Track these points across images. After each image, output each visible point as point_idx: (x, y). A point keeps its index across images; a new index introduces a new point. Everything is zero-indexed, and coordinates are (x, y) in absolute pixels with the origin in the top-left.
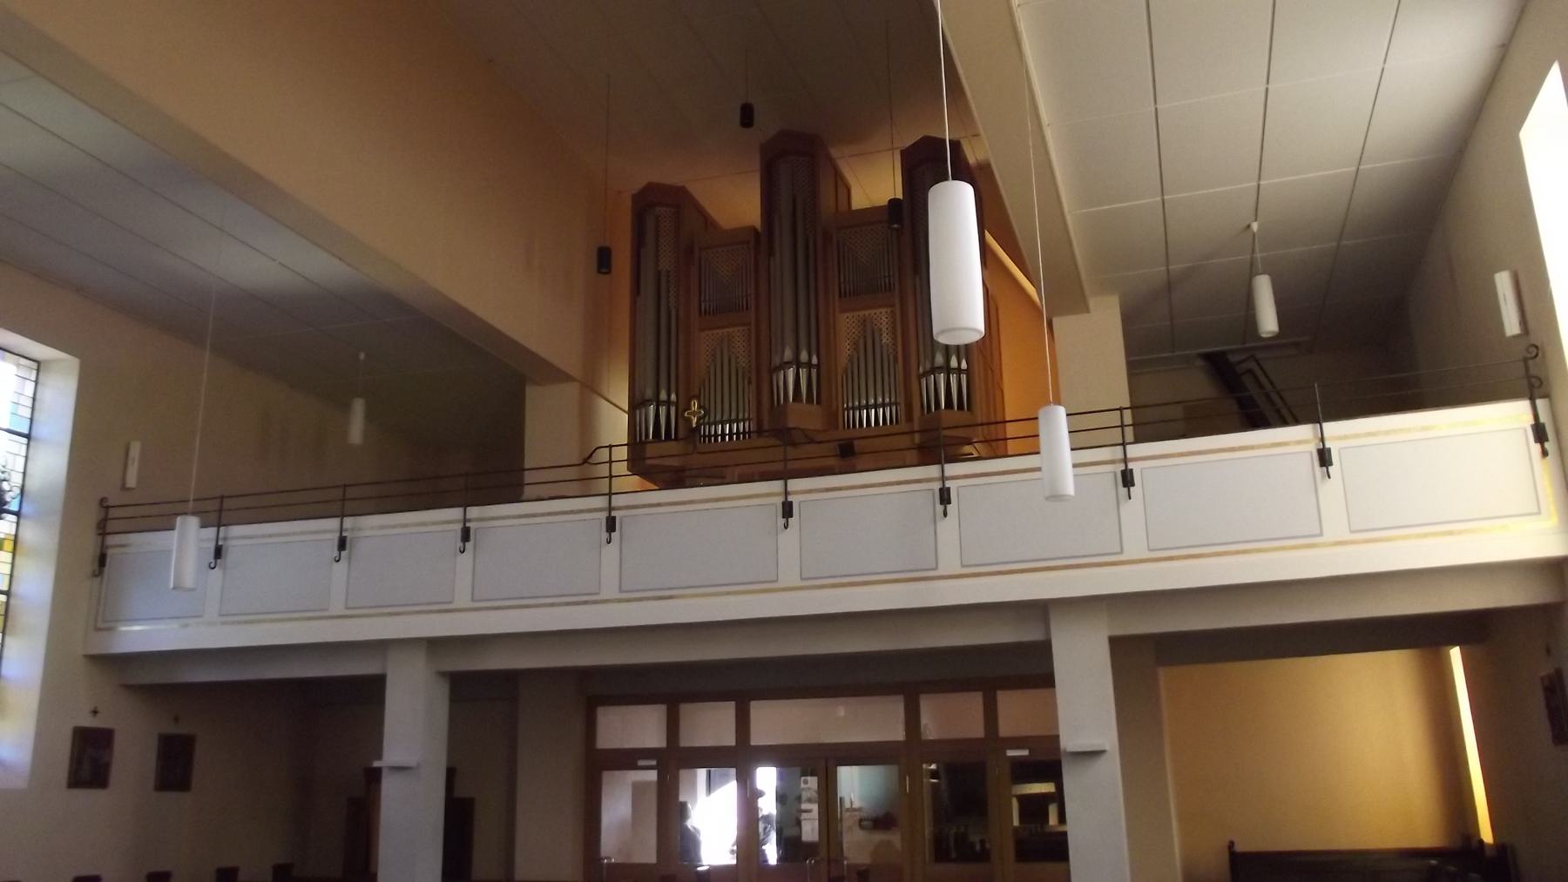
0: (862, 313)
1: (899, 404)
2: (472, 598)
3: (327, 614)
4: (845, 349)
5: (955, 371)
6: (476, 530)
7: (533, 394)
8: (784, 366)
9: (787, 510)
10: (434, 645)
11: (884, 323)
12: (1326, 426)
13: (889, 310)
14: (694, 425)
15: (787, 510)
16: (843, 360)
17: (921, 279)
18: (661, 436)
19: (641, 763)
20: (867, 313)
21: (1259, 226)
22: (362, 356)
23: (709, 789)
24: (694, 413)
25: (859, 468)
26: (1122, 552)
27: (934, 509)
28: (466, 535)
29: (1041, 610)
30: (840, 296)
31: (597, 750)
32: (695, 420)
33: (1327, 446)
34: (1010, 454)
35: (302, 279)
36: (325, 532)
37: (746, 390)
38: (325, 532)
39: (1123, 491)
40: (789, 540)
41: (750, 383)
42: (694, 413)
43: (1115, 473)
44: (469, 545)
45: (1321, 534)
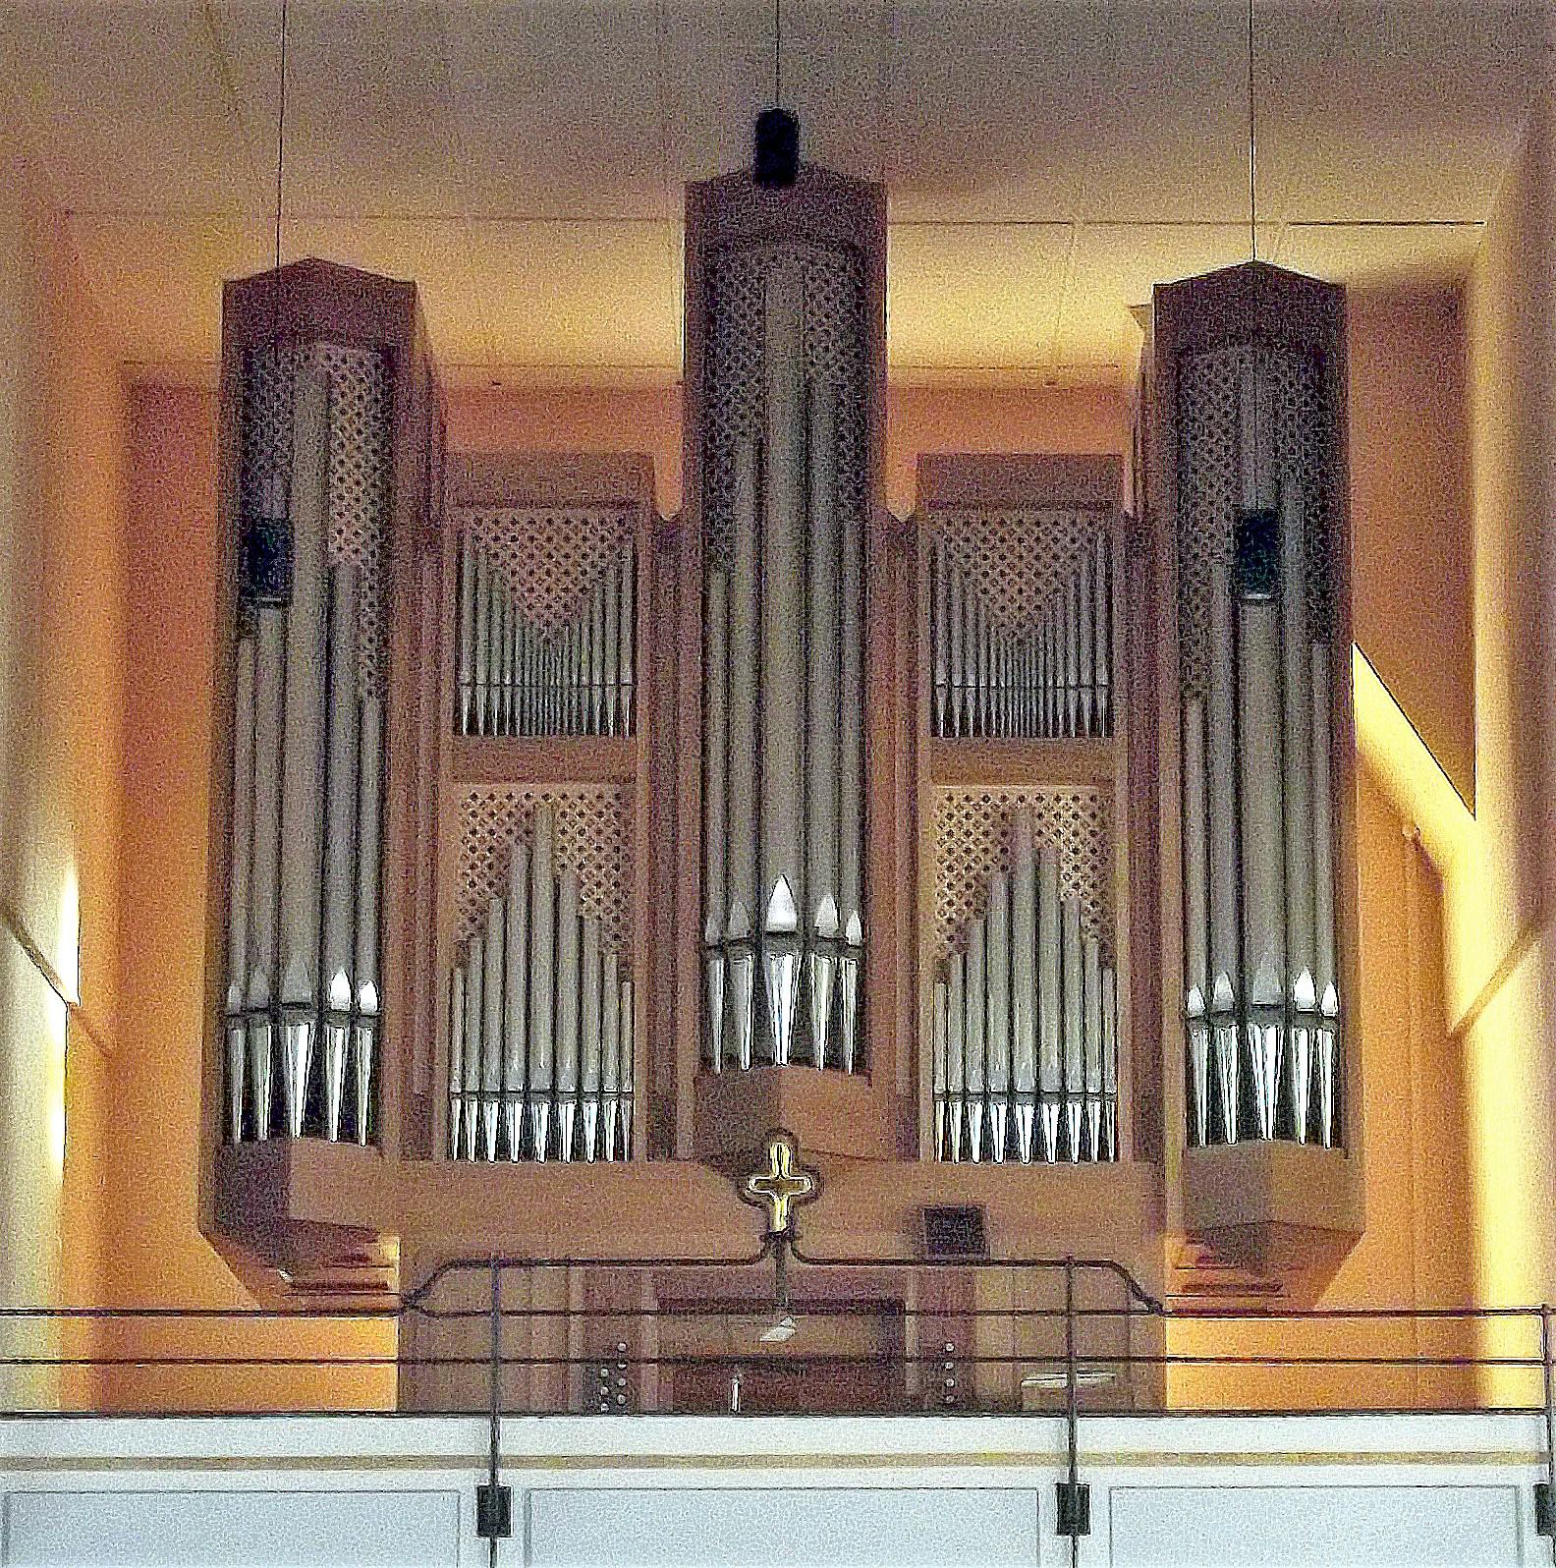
4: (940, 898)
8: (760, 939)
16: (933, 940)
20: (1013, 791)
32: (781, 1206)
42: (777, 1186)
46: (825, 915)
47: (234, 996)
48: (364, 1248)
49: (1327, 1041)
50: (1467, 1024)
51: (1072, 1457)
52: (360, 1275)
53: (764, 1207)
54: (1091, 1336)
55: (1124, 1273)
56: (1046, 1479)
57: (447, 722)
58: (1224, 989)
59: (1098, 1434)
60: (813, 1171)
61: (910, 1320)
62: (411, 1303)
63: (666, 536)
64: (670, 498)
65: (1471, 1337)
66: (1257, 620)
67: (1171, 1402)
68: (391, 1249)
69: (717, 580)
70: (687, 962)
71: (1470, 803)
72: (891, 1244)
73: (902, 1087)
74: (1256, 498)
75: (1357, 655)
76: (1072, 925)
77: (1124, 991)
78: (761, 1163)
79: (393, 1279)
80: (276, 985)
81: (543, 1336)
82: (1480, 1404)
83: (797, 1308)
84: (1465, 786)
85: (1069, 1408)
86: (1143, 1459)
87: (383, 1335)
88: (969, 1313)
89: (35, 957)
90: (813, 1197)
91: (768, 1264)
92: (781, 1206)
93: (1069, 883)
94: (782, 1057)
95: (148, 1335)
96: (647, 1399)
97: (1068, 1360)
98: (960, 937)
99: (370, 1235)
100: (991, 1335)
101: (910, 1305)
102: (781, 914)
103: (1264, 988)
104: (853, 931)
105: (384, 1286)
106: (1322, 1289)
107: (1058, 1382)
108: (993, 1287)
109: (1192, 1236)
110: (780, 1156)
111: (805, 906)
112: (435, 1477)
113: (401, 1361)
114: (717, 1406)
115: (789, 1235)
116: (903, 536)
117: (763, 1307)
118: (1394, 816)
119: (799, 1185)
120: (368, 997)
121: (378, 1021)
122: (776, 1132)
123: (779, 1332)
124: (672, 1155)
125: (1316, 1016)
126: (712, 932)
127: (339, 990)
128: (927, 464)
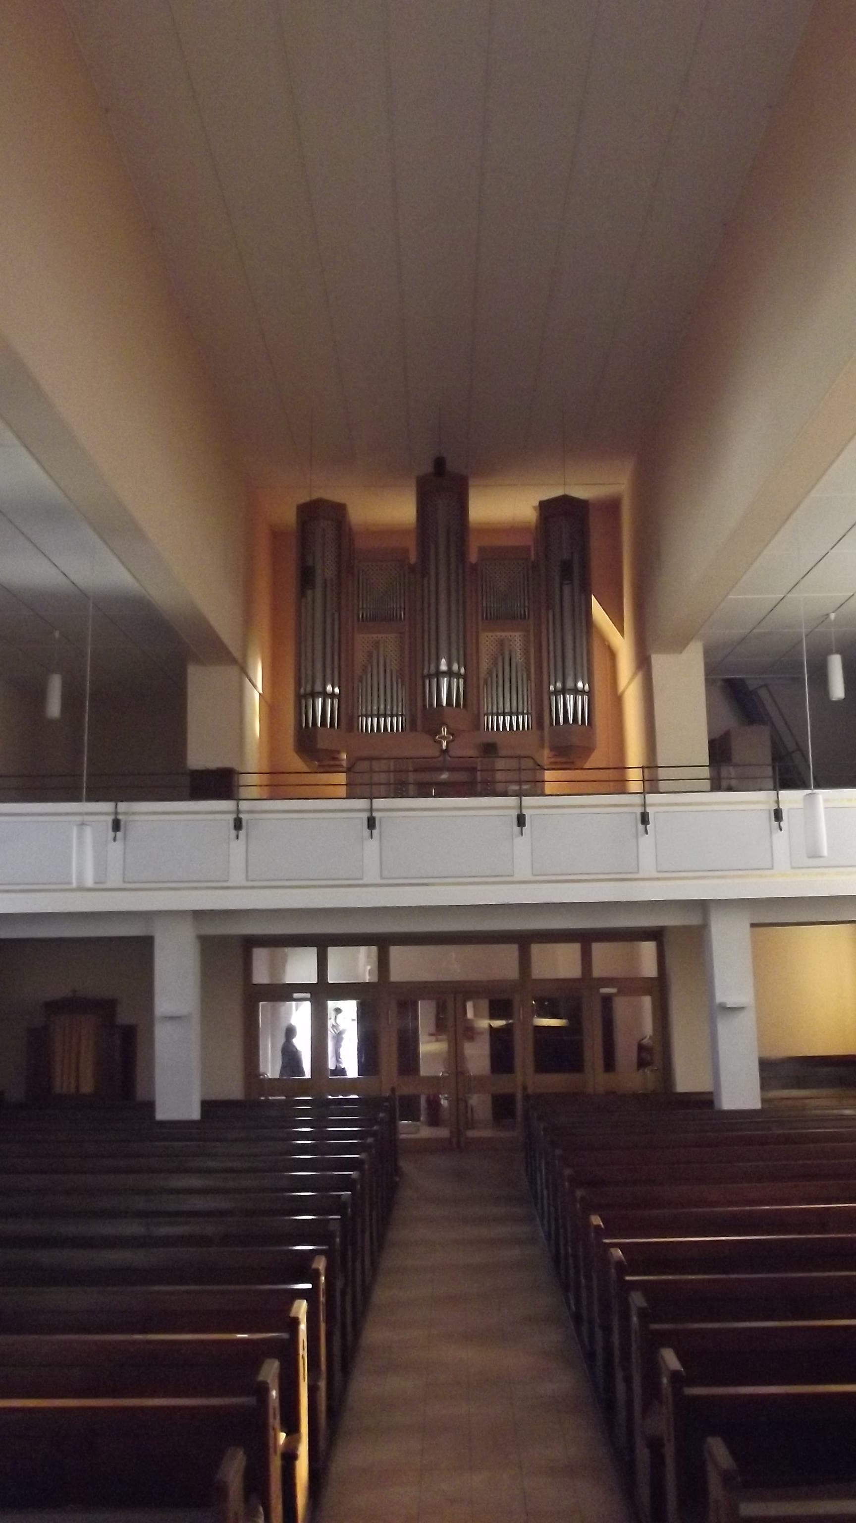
2: (247, 876)
4: (485, 664)
8: (439, 674)
9: (521, 821)
10: (198, 915)
11: (518, 645)
12: (120, 804)
14: (444, 747)
15: (521, 821)
16: (483, 674)
19: (296, 995)
22: (57, 634)
23: (297, 1009)
24: (444, 738)
25: (411, 795)
26: (638, 872)
27: (637, 827)
29: (703, 906)
31: (595, 979)
32: (444, 744)
33: (781, 807)
34: (661, 791)
36: (758, 802)
38: (758, 802)
39: (641, 827)
40: (522, 844)
42: (444, 738)
43: (770, 811)
44: (242, 833)
45: (772, 868)
46: (455, 667)
47: (302, 690)
48: (336, 756)
49: (586, 698)
50: (623, 693)
51: (521, 807)
52: (337, 763)
53: (441, 744)
54: (525, 776)
55: (532, 758)
56: (514, 813)
57: (356, 618)
58: (559, 685)
59: (527, 801)
60: (453, 735)
61: (479, 773)
62: (349, 770)
63: (412, 569)
64: (413, 558)
65: (624, 775)
66: (567, 590)
67: (547, 792)
68: (344, 756)
70: (420, 682)
72: (471, 752)
73: (476, 712)
74: (566, 556)
75: (593, 597)
76: (519, 669)
77: (533, 685)
78: (439, 732)
79: (344, 764)
81: (383, 778)
82: (626, 792)
83: (451, 769)
84: (621, 631)
85: (519, 794)
86: (540, 807)
87: (342, 778)
88: (494, 770)
89: (250, 680)
90: (453, 741)
91: (441, 759)
92: (444, 744)
93: (518, 658)
94: (444, 704)
95: (282, 778)
96: (411, 793)
97: (520, 783)
98: (490, 673)
99: (339, 752)
100: (499, 776)
101: (479, 768)
102: (444, 667)
103: (570, 684)
104: (462, 671)
105: (342, 766)
106: (585, 763)
108: (500, 764)
109: (552, 749)
110: (444, 731)
111: (449, 665)
112: (507, 812)
113: (544, 781)
114: (428, 795)
115: (446, 751)
116: (474, 568)
117: (440, 770)
118: (604, 640)
119: (449, 737)
120: (337, 690)
121: (339, 696)
122: (444, 724)
123: (444, 776)
124: (416, 730)
125: (583, 692)
126: (426, 672)
127: (329, 688)
128: (481, 549)
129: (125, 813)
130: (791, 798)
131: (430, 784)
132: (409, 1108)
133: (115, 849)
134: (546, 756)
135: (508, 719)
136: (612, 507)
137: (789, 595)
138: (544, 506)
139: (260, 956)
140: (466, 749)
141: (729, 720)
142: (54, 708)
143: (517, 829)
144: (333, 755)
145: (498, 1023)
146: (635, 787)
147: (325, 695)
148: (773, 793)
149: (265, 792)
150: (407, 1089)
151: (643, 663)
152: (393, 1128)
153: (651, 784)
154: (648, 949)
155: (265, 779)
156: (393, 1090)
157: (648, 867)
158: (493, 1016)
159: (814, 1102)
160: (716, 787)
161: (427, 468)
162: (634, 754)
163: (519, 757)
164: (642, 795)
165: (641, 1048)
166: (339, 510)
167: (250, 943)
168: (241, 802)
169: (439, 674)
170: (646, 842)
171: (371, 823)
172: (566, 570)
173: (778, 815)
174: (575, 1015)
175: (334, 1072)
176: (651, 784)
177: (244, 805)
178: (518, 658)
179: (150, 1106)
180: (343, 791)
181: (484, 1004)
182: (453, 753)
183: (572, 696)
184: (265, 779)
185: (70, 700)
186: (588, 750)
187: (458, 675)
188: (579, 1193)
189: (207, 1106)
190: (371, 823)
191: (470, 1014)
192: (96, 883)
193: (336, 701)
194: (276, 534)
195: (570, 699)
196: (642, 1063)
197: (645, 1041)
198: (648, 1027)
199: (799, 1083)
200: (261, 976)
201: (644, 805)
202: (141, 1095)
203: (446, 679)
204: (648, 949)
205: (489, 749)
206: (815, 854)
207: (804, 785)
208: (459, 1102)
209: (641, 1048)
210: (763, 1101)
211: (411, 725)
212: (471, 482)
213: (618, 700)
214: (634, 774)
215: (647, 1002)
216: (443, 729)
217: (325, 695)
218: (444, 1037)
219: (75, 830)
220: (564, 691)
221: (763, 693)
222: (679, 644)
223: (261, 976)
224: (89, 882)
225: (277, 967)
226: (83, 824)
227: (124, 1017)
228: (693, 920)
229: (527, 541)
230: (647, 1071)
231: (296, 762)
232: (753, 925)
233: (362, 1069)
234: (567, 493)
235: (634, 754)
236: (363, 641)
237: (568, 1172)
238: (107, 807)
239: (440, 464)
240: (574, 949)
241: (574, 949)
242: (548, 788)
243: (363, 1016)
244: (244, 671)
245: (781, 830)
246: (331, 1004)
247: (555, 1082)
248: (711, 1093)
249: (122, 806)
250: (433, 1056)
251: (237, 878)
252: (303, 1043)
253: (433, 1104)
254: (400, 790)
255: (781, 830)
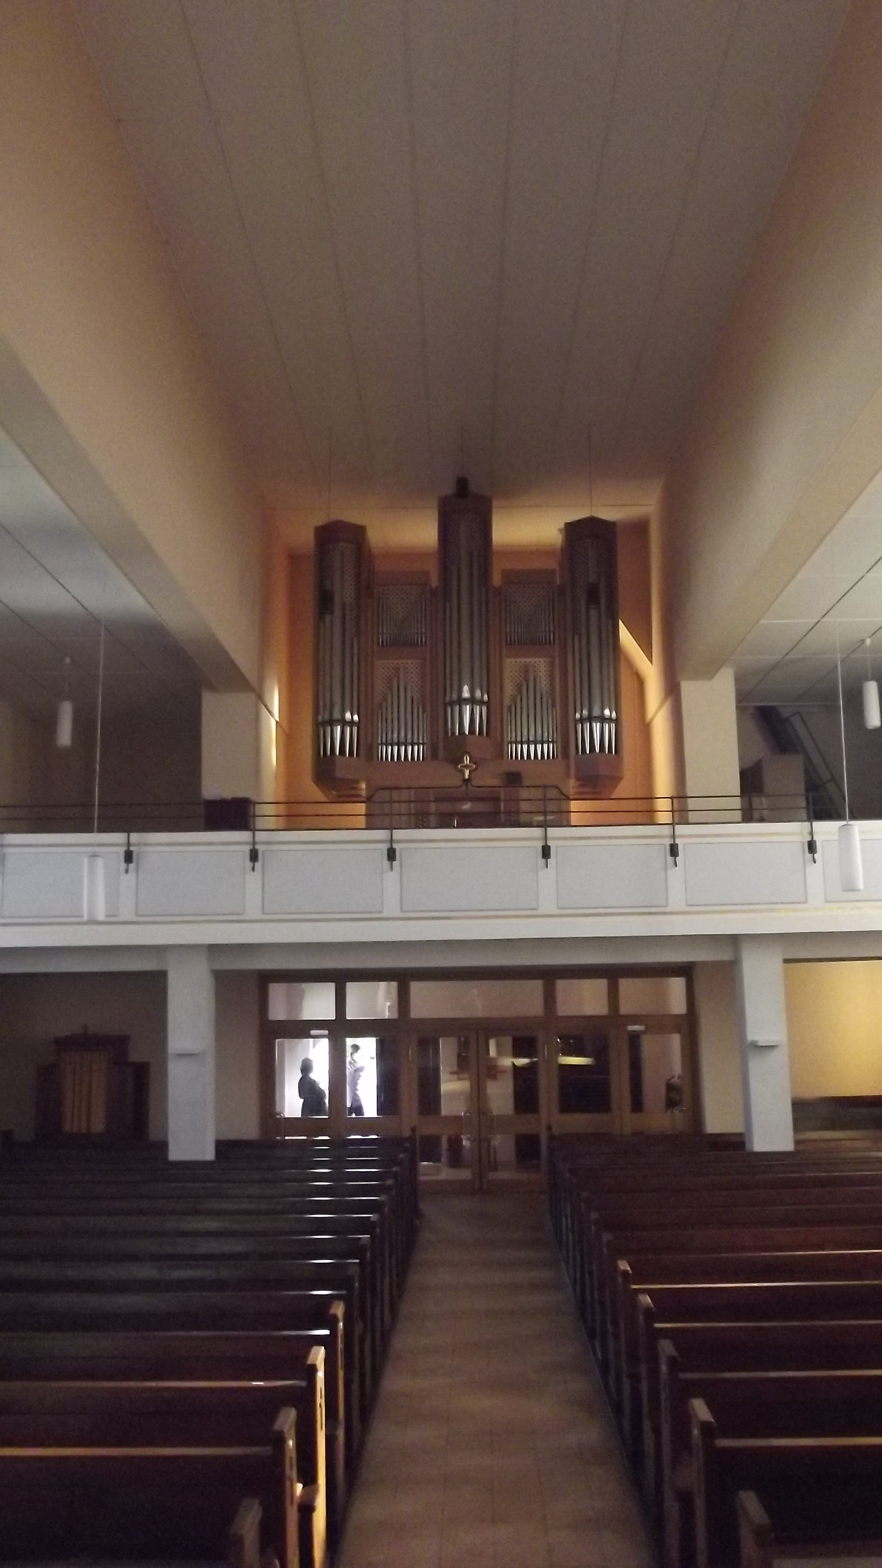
0: (523, 660)
1: (556, 742)
3: (114, 919)
4: (509, 689)
5: (614, 721)
6: (263, 852)
7: (209, 701)
8: (461, 701)
9: (546, 852)
10: (213, 950)
13: (548, 660)
15: (546, 852)
16: (507, 701)
17: (580, 639)
18: (345, 755)
19: (313, 1032)
20: (528, 660)
21: (872, 643)
22: (68, 660)
23: (314, 1046)
28: (254, 856)
29: (735, 940)
30: (507, 644)
32: (467, 773)
35: (73, 600)
37: (421, 716)
39: (670, 859)
40: (548, 876)
41: (424, 711)
42: (466, 767)
44: (258, 865)
46: (478, 694)
54: (552, 806)
56: (539, 844)
58: (585, 712)
59: (552, 832)
62: (369, 800)
64: (434, 582)
69: (448, 605)
71: (652, 663)
80: (331, 714)
85: (544, 825)
92: (467, 773)
93: (544, 684)
97: (545, 813)
98: (514, 700)
99: (357, 782)
100: (524, 806)
102: (466, 694)
107: (541, 818)
108: (524, 793)
109: (578, 778)
110: (467, 760)
111: (472, 691)
116: (498, 591)
117: (464, 799)
120: (356, 718)
123: (467, 806)
125: (610, 720)
129: (138, 845)
130: (825, 830)
131: (451, 815)
132: (429, 1148)
133: (128, 880)
134: (571, 785)
135: (532, 747)
136: (640, 528)
137: (823, 620)
138: (573, 530)
139: (277, 992)
140: (489, 779)
141: (760, 748)
142: (65, 735)
143: (541, 861)
144: (352, 784)
145: (522, 1061)
146: (664, 817)
147: (343, 722)
148: (807, 824)
149: (281, 822)
150: (429, 1128)
151: (672, 690)
152: (413, 1168)
153: (681, 815)
154: (677, 985)
155: (281, 809)
156: (413, 1130)
157: (677, 900)
158: (516, 1055)
159: (859, 1144)
160: (748, 816)
161: (449, 489)
162: (663, 784)
163: (545, 787)
164: (671, 827)
165: (670, 1087)
166: (359, 532)
167: (266, 978)
168: (257, 833)
169: (461, 701)
170: (676, 875)
171: (391, 855)
172: (593, 596)
173: (812, 847)
174: (601, 1054)
175: (351, 1110)
176: (681, 815)
177: (261, 836)
178: (543, 685)
179: (163, 1146)
180: (362, 821)
181: (508, 1041)
182: (475, 782)
183: (598, 724)
184: (281, 809)
185: (83, 726)
186: (616, 779)
187: (481, 702)
188: (606, 1237)
189: (223, 1147)
190: (391, 855)
191: (493, 1052)
192: (107, 916)
193: (355, 729)
194: (294, 558)
195: (597, 727)
196: (671, 1104)
197: (675, 1080)
198: (677, 1067)
199: (833, 1125)
200: (278, 1012)
201: (674, 836)
202: (154, 1135)
203: (468, 706)
204: (677, 985)
205: (514, 779)
206: (849, 887)
207: (839, 817)
208: (481, 1141)
209: (670, 1087)
210: (797, 1142)
211: (433, 753)
212: (495, 503)
213: (646, 729)
214: (663, 805)
215: (676, 1040)
216: (465, 758)
217: (343, 722)
218: (466, 1076)
219: (86, 861)
220: (590, 719)
221: (796, 722)
222: (708, 670)
223: (278, 1012)
224: (101, 917)
225: (295, 1002)
226: (94, 856)
227: (135, 1056)
228: (724, 955)
229: (552, 564)
230: (676, 1112)
231: (315, 792)
232: (786, 961)
233: (382, 1107)
234: (593, 515)
235: (663, 784)
236: (383, 667)
237: (594, 1216)
238: (119, 837)
239: (462, 485)
240: (602, 984)
241: (602, 984)
242: (574, 818)
243: (383, 1053)
244: (261, 698)
245: (815, 862)
246: (350, 1041)
247: (578, 1122)
248: (741, 1135)
249: (135, 837)
250: (452, 1095)
251: (253, 912)
252: (321, 1077)
253: (455, 1144)
254: (421, 821)
255: (815, 862)
